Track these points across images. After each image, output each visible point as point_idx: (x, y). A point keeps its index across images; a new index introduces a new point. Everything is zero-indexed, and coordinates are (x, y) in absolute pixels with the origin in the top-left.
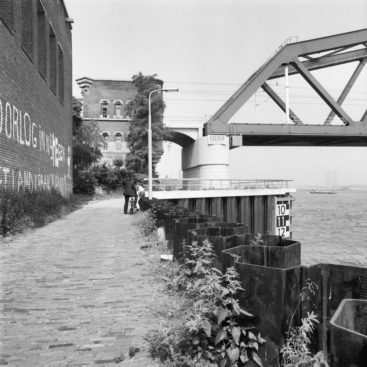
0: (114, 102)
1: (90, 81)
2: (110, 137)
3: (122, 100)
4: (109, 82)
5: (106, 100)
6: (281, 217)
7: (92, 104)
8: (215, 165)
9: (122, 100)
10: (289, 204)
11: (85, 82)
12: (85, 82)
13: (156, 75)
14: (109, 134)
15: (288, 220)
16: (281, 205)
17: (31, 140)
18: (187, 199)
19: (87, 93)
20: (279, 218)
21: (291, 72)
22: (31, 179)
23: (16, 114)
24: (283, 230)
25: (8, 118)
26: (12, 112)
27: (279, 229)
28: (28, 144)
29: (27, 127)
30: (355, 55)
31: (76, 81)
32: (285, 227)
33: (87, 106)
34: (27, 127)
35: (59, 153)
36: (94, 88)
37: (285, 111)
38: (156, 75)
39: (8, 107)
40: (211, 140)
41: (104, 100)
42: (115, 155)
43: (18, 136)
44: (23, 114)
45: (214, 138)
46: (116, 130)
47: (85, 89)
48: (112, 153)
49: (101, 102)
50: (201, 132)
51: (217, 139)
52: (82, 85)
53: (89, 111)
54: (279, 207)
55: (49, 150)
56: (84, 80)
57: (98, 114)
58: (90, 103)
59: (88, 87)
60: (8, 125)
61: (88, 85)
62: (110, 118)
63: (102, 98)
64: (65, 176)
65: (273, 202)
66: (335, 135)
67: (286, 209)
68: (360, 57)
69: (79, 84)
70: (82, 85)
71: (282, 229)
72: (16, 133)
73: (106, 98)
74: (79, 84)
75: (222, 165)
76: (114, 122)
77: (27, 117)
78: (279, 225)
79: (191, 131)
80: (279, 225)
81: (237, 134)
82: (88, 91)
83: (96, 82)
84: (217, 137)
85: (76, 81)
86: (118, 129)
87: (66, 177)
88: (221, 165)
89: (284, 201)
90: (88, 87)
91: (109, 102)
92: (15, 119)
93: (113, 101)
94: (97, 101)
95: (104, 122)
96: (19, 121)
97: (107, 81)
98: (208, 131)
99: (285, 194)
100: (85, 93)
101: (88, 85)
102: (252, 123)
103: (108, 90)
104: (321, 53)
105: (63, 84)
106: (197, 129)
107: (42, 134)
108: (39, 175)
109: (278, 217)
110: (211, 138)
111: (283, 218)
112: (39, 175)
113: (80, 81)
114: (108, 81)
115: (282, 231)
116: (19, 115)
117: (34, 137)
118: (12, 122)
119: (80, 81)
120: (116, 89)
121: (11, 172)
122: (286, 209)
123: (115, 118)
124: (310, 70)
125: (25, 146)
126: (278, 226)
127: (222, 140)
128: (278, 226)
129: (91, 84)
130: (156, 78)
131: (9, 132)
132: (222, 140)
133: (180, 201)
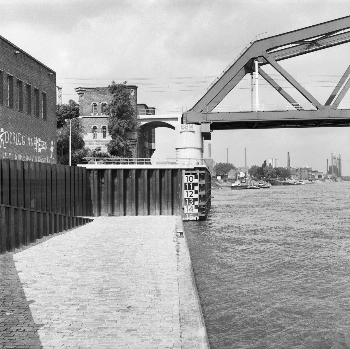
0: (101, 104)
1: (84, 89)
6: (189, 184)
11: (80, 90)
12: (80, 90)
14: (97, 127)
16: (189, 176)
17: (22, 142)
18: (110, 169)
20: (187, 184)
21: (285, 56)
23: (14, 135)
24: (191, 193)
25: (11, 138)
26: (13, 135)
27: (187, 192)
28: (20, 144)
29: (20, 138)
30: (206, 83)
34: (20, 138)
35: (42, 145)
39: (11, 134)
43: (15, 142)
44: (17, 134)
45: (184, 126)
46: (102, 124)
47: (81, 95)
48: (99, 141)
49: (92, 104)
50: (180, 120)
51: (187, 127)
52: (79, 92)
53: (84, 110)
54: (187, 177)
55: (33, 145)
56: (80, 89)
59: (83, 94)
60: (11, 139)
62: (99, 115)
63: (93, 101)
64: (48, 157)
65: (181, 174)
66: (302, 119)
68: (339, 42)
70: (79, 92)
71: (190, 192)
72: (14, 141)
73: (95, 101)
74: (77, 91)
75: (192, 149)
76: (101, 118)
77: (19, 134)
78: (187, 189)
79: (169, 121)
81: (207, 122)
83: (88, 90)
84: (183, 126)
85: (75, 89)
86: (104, 123)
87: (49, 158)
88: (190, 149)
89: (192, 173)
90: (83, 94)
91: (97, 104)
92: (14, 137)
93: (100, 102)
94: (89, 104)
95: (94, 119)
96: (15, 137)
98: (184, 120)
100: (81, 98)
102: (223, 112)
104: (293, 44)
105: (46, 109)
106: (177, 118)
107: (28, 139)
108: (26, 156)
109: (185, 184)
110: (182, 127)
111: (191, 184)
112: (26, 156)
113: (77, 90)
115: (189, 194)
116: (16, 136)
117: (23, 141)
118: (13, 138)
119: (77, 90)
121: (12, 155)
124: (277, 60)
125: (18, 145)
126: (186, 189)
127: (191, 128)
128: (186, 189)
129: (85, 91)
130: (127, 84)
131: (11, 142)
132: (191, 128)
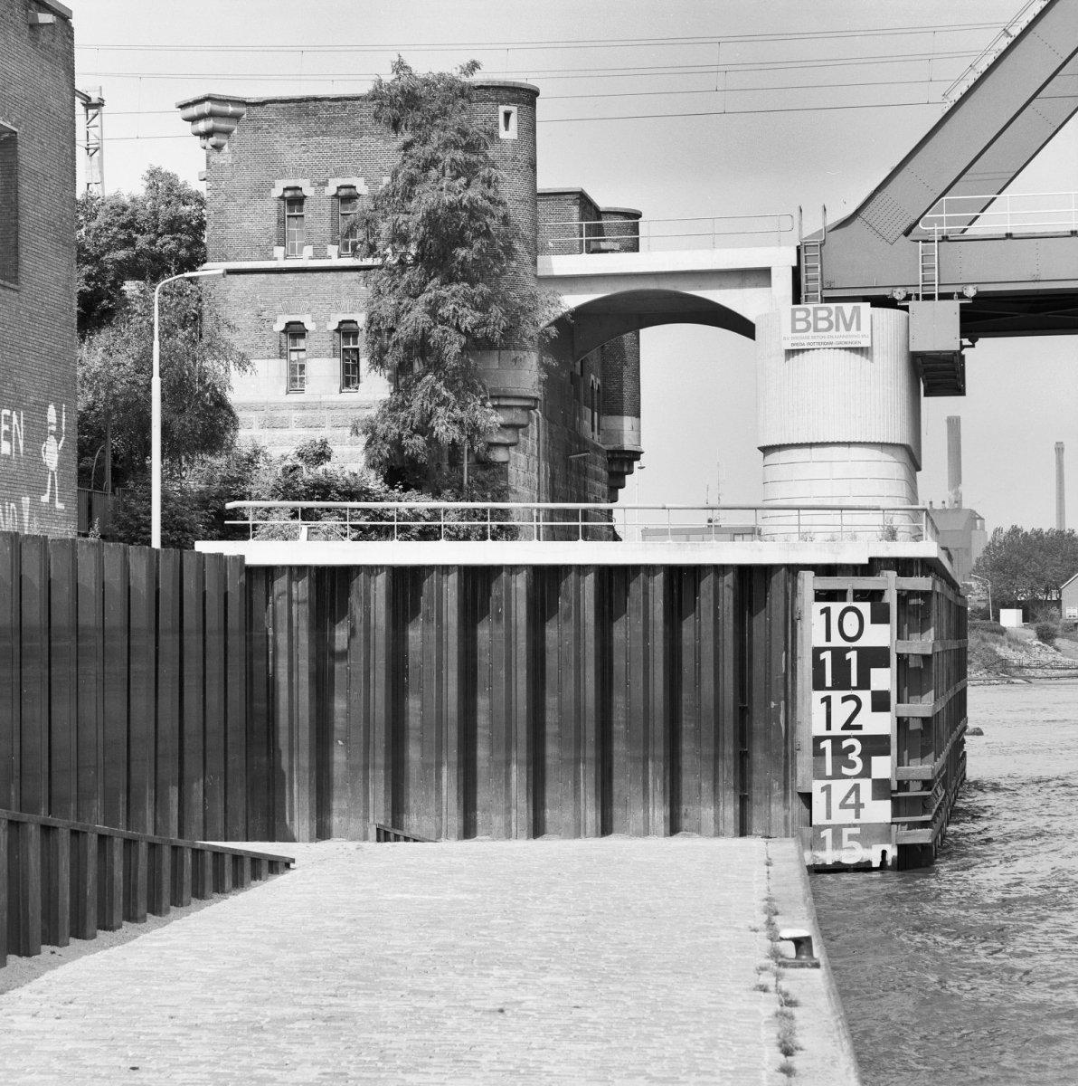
0: (331, 190)
1: (230, 109)
2: (312, 338)
3: (362, 180)
4: (311, 105)
5: (299, 183)
6: (839, 654)
7: (240, 201)
8: (814, 450)
9: (362, 180)
10: (887, 605)
11: (211, 115)
12: (211, 115)
13: (474, 66)
14: (309, 326)
15: (887, 665)
16: (837, 608)
18: (382, 567)
19: (225, 157)
20: (827, 656)
22: (14, 514)
24: (852, 705)
27: (827, 700)
31: (182, 107)
32: (865, 696)
33: (222, 212)
36: (249, 134)
37: (978, 216)
38: (474, 66)
40: (794, 330)
41: (291, 183)
42: (335, 413)
45: (811, 319)
46: (338, 308)
47: (213, 140)
48: (317, 406)
50: (782, 283)
52: (202, 126)
54: (827, 611)
56: (206, 107)
57: (265, 241)
58: (231, 197)
59: (227, 133)
61: (223, 125)
62: (316, 257)
63: (283, 175)
64: (26, 501)
65: (791, 594)
67: (874, 621)
69: (193, 120)
70: (202, 126)
71: (845, 699)
73: (298, 173)
74: (193, 120)
75: (854, 450)
78: (829, 683)
80: (829, 683)
81: (945, 290)
82: (226, 148)
85: (182, 107)
86: (346, 302)
87: (35, 504)
89: (856, 592)
90: (227, 133)
94: (261, 190)
95: (290, 277)
97: (300, 100)
99: (866, 562)
101: (223, 125)
103: (304, 140)
105: (17, 225)
109: (817, 651)
110: (794, 320)
111: (852, 656)
113: (194, 111)
114: (307, 100)
119: (194, 111)
120: (339, 134)
122: (874, 621)
123: (335, 256)
127: (848, 328)
128: (818, 684)
132: (848, 328)
133: (358, 574)
